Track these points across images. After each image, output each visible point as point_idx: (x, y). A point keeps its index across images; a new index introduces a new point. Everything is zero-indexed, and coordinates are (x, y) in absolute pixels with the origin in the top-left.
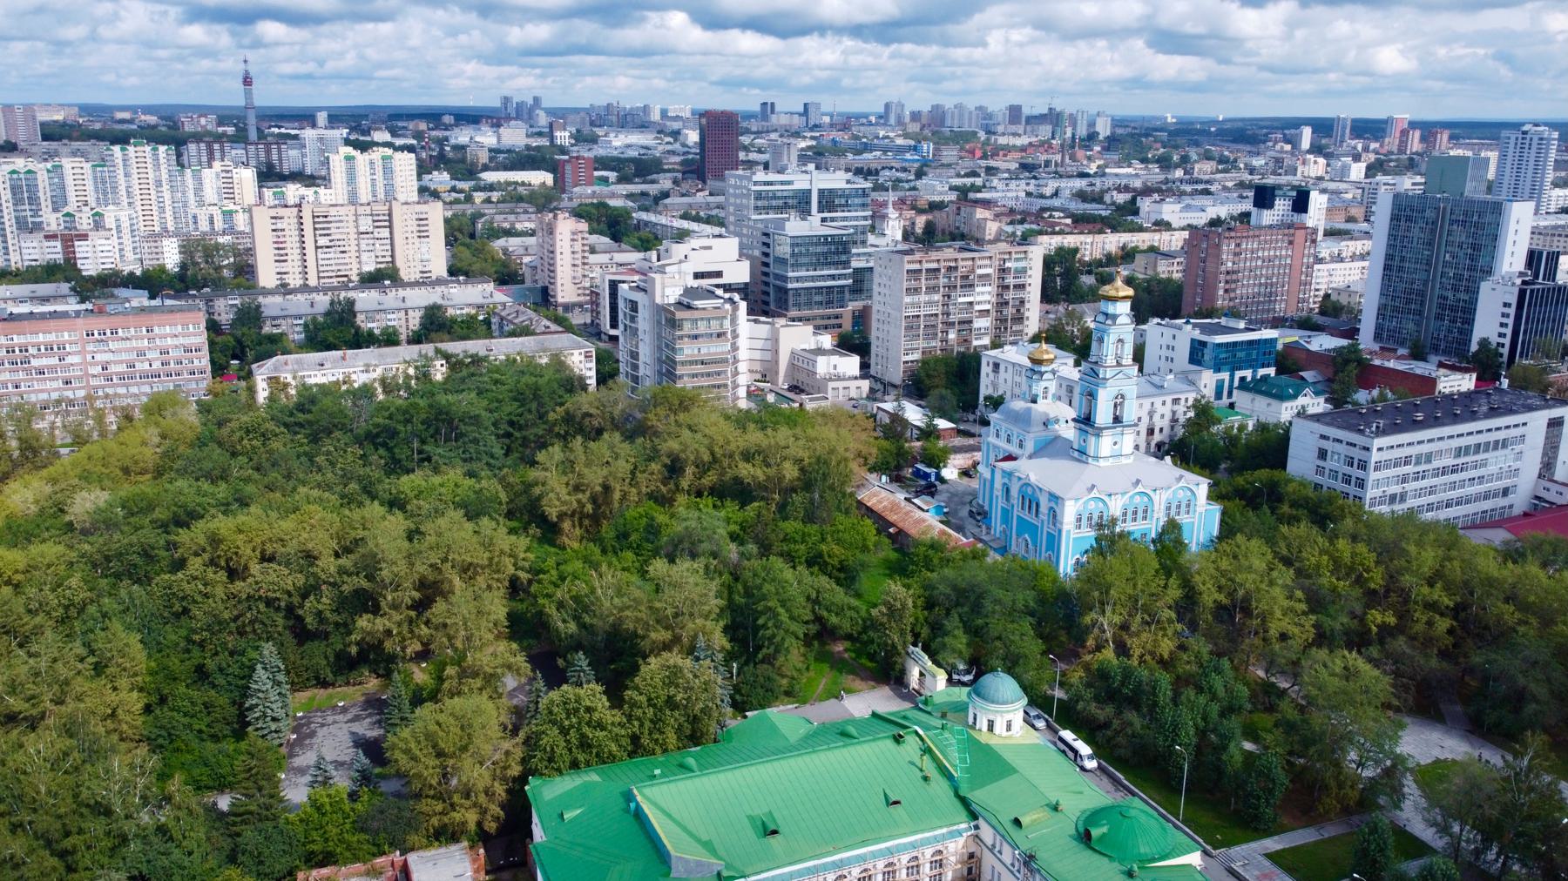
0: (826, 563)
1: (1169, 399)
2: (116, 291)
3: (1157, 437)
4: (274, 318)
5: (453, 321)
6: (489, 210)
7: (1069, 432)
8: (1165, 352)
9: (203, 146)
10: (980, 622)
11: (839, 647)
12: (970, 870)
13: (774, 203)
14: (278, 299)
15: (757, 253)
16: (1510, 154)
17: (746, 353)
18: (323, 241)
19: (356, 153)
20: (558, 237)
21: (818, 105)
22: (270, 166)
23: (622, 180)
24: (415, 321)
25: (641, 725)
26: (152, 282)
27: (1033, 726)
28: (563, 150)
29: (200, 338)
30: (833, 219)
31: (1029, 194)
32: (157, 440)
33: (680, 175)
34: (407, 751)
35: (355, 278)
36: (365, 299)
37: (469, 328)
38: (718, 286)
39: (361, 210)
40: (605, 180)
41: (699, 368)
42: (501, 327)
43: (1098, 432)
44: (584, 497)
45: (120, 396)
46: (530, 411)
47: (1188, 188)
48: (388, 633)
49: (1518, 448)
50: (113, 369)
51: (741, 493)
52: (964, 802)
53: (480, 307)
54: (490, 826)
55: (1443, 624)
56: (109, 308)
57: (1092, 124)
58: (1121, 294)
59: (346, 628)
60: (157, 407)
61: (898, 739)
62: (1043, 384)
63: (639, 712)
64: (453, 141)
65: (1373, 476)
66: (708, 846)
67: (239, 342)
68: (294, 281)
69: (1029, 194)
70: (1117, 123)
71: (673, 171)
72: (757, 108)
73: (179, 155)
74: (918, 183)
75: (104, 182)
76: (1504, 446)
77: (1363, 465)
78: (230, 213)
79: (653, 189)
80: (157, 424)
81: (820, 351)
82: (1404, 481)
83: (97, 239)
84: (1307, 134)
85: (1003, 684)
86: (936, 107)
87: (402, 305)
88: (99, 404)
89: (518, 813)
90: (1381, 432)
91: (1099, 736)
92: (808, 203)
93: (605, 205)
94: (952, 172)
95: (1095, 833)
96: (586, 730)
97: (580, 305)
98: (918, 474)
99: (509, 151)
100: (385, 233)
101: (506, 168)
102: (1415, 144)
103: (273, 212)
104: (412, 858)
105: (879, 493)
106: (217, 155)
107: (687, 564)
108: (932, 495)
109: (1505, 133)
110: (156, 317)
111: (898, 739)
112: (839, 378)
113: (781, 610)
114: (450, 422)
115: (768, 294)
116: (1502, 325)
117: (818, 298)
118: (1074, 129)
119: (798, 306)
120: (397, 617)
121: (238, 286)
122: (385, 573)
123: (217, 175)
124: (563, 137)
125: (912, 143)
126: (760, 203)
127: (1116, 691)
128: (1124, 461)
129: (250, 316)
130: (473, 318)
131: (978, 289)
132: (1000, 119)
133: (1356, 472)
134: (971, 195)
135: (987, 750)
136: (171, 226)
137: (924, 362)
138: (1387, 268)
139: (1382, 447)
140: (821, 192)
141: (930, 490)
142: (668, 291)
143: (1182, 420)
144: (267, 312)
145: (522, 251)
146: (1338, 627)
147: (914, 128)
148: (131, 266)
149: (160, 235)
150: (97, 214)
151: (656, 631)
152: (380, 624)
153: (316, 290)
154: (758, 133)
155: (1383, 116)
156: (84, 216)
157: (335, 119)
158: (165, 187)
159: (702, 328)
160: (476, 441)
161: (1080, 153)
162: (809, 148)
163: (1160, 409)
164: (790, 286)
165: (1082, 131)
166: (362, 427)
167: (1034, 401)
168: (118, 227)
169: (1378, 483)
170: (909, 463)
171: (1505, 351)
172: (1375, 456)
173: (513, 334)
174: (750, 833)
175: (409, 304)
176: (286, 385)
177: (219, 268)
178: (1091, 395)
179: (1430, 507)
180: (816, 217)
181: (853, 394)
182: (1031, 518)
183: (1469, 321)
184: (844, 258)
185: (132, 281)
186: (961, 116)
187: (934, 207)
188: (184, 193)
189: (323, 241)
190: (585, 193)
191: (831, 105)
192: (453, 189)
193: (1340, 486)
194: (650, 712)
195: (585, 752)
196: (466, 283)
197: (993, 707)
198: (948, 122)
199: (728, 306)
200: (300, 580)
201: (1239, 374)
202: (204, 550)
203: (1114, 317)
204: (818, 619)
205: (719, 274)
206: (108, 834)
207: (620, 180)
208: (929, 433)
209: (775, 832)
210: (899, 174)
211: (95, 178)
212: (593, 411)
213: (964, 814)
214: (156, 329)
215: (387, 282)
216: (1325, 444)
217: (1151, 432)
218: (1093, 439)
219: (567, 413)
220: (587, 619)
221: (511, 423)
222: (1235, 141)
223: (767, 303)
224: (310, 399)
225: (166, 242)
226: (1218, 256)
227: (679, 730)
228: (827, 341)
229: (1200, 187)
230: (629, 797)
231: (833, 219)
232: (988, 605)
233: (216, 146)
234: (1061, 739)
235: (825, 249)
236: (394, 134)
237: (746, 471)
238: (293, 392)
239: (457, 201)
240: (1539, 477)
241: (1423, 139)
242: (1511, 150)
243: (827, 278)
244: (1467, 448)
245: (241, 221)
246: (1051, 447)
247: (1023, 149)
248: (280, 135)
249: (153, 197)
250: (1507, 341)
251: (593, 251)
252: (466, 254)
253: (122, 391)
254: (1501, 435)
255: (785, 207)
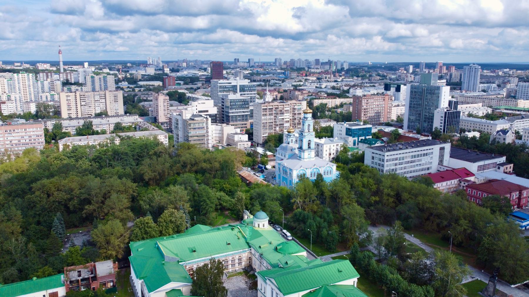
0: (225, 190)
1: (335, 145)
2: (15, 119)
3: (332, 156)
4: (66, 127)
5: (124, 127)
6: (140, 94)
7: (297, 151)
8: (339, 132)
9: (45, 74)
10: (264, 202)
11: (227, 212)
12: (250, 262)
13: (225, 89)
14: (68, 121)
15: (220, 105)
16: (466, 73)
17: (213, 134)
18: (83, 103)
19: (95, 76)
20: (159, 101)
21: (253, 59)
22: (67, 80)
23: (185, 84)
24: (112, 127)
25: (162, 228)
26: (28, 117)
27: (277, 230)
28: (167, 75)
29: (42, 133)
30: (244, 94)
31: (316, 87)
32: (27, 162)
33: (204, 82)
34: (96, 235)
35: (94, 115)
36: (96, 121)
37: (129, 129)
38: (207, 115)
39: (96, 93)
40: (179, 84)
41: (196, 138)
42: (139, 128)
43: (304, 151)
44: (156, 174)
45: (15, 151)
46: (144, 152)
47: (368, 85)
48: (95, 210)
49: (431, 156)
50: (13, 142)
51: (203, 172)
52: (248, 243)
53: (133, 123)
54: (120, 256)
55: (391, 200)
56: (12, 123)
57: (342, 65)
58: (308, 111)
59: (82, 209)
60: (27, 152)
61: (232, 229)
62: (291, 139)
63: (162, 224)
64: (130, 72)
65: (386, 164)
66: (176, 255)
67: (54, 134)
68: (74, 116)
69: (316, 87)
70: (351, 64)
71: (203, 81)
72: (233, 60)
73: (36, 77)
74: (282, 84)
75: (11, 85)
76: (426, 155)
77: (383, 161)
78: (53, 95)
79: (194, 87)
80: (28, 157)
81: (236, 134)
82: (396, 165)
83: (9, 104)
84: (411, 67)
85: (263, 214)
86: (292, 60)
87: (108, 123)
88: (9, 153)
89: (128, 252)
90: (389, 151)
91: (294, 231)
92: (236, 89)
93: (178, 92)
94: (294, 80)
95: (278, 248)
96: (146, 229)
97: (166, 123)
98: (259, 167)
99: (148, 75)
100: (104, 100)
101: (147, 81)
102: (444, 71)
103: (67, 94)
104: (97, 264)
105: (247, 172)
106: (50, 77)
107: (179, 187)
108: (262, 173)
109: (464, 67)
110: (27, 126)
111: (232, 229)
112: (242, 141)
113: (207, 200)
114: (118, 154)
115: (223, 117)
116: (441, 123)
117: (239, 119)
118: (336, 67)
119: (233, 121)
120: (97, 205)
121: (55, 118)
122: (93, 193)
123: (49, 83)
124: (167, 70)
125: (283, 71)
126: (221, 89)
127: (301, 220)
128: (312, 159)
129: (58, 127)
130: (131, 126)
131: (285, 114)
132: (313, 64)
133: (381, 163)
134: (298, 88)
135: (257, 231)
136: (33, 99)
137: (268, 136)
138: (410, 107)
139: (388, 155)
140: (240, 86)
141: (262, 172)
142: (187, 115)
143: (339, 150)
144: (64, 125)
145: (149, 106)
146: (363, 201)
147: (284, 66)
148: (20, 112)
149: (29, 102)
150: (9, 96)
151: (170, 205)
152: (92, 207)
153: (80, 118)
154: (233, 69)
155: (435, 62)
156: (4, 96)
157: (91, 64)
158: (32, 87)
159: (197, 126)
160: (126, 160)
161: (337, 74)
162: (249, 73)
163: (332, 148)
164: (230, 115)
165: (339, 67)
166: (91, 157)
167: (289, 144)
168: (16, 100)
169: (387, 166)
170: (256, 163)
171: (442, 131)
172: (386, 158)
173: (142, 130)
174: (188, 252)
175: (110, 122)
176: (69, 146)
177: (49, 112)
178: (302, 141)
179: (405, 173)
180: (239, 94)
181: (246, 146)
182: (285, 176)
183: (432, 122)
184: (247, 106)
185: (20, 117)
186: (300, 62)
187: (285, 91)
188: (38, 88)
189: (83, 103)
190: (172, 88)
191: (257, 59)
192: (128, 87)
193: (378, 167)
194: (165, 224)
195: (146, 235)
196: (129, 116)
197: (259, 220)
198: (296, 65)
199: (205, 119)
200: (69, 196)
201: (360, 138)
202: (40, 189)
203: (307, 118)
204: (221, 204)
205: (207, 111)
206: (11, 259)
207: (185, 84)
208: (266, 156)
209: (195, 251)
210: (276, 81)
211: (8, 84)
212: (163, 151)
213: (247, 247)
214: (28, 130)
215: (104, 116)
216: (374, 155)
217: (330, 154)
218: (302, 153)
219: (155, 152)
220: (152, 204)
221: (139, 156)
222: (389, 70)
223: (223, 120)
224: (75, 149)
225: (31, 104)
226: (361, 104)
227: (173, 229)
228: (238, 131)
229: (372, 85)
230: (157, 244)
231: (244, 94)
232: (266, 198)
233: (49, 74)
234: (283, 233)
235: (241, 103)
236: (110, 70)
237: (204, 165)
238: (71, 148)
239: (129, 91)
240: (439, 164)
241: (447, 69)
242: (467, 72)
243: (240, 112)
244: (415, 156)
245: (56, 97)
246: (293, 156)
247: (319, 73)
248: (71, 70)
249: (27, 90)
250: (442, 128)
251: (171, 106)
252: (130, 107)
253: (17, 149)
254: (425, 152)
255: (229, 91)
